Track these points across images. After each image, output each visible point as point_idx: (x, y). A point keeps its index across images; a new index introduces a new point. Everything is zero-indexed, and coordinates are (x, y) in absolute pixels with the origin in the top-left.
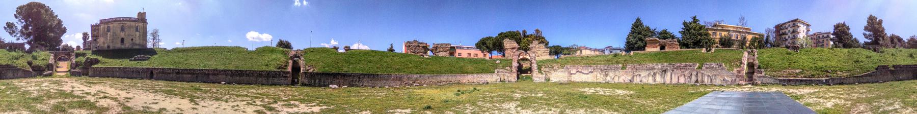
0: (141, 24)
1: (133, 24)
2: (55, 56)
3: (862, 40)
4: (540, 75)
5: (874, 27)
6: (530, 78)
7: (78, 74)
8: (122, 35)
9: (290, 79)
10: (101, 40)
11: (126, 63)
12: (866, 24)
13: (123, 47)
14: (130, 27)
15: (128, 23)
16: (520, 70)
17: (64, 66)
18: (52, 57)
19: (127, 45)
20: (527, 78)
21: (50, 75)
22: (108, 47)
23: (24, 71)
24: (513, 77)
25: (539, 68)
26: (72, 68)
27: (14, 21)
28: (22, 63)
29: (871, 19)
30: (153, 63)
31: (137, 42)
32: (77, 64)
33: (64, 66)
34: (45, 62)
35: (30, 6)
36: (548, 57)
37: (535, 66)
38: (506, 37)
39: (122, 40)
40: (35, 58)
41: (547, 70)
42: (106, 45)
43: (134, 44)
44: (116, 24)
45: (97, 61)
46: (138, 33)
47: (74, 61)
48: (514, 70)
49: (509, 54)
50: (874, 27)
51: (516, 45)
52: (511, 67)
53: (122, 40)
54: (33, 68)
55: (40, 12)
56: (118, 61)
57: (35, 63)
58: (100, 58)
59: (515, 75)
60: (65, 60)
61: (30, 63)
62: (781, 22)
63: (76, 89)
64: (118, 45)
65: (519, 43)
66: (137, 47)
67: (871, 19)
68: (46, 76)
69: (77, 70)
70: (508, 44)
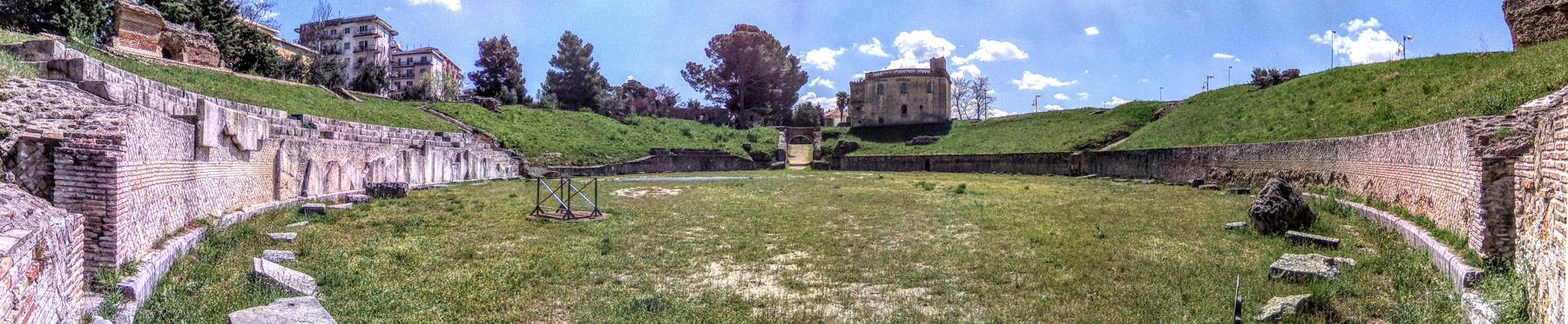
0: (935, 80)
1: (922, 80)
2: (787, 135)
3: (535, 100)
5: (573, 54)
7: (825, 167)
8: (904, 99)
9: (1505, 179)
10: (867, 109)
11: (901, 149)
12: (555, 51)
13: (905, 120)
14: (916, 85)
15: (914, 79)
17: (800, 155)
18: (782, 138)
19: (913, 116)
21: (782, 167)
22: (881, 120)
23: (742, 160)
26: (815, 157)
28: (733, 146)
29: (569, 41)
30: (941, 147)
31: (930, 111)
32: (824, 152)
33: (800, 155)
34: (770, 147)
35: (574, 37)
39: (904, 109)
40: (752, 139)
42: (876, 118)
43: (924, 115)
44: (891, 81)
45: (855, 147)
46: (930, 96)
47: (819, 147)
50: (573, 54)
53: (904, 109)
54: (752, 155)
55: (756, 53)
56: (888, 146)
57: (755, 147)
58: (858, 141)
60: (802, 141)
61: (747, 148)
64: (897, 118)
66: (931, 120)
67: (569, 41)
68: (775, 168)
69: (823, 161)
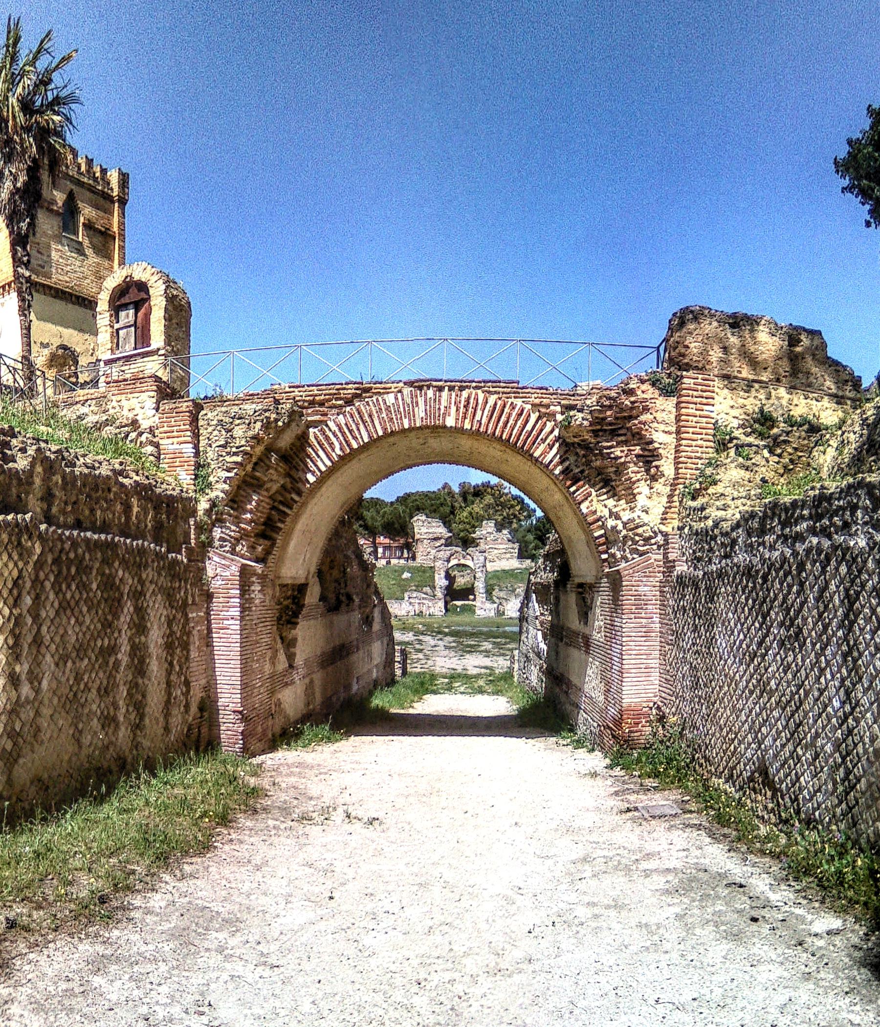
4: (488, 605)
6: (471, 610)
16: (453, 593)
20: (464, 608)
24: (437, 608)
25: (489, 592)
27: (868, 218)
36: (514, 564)
37: (480, 586)
38: (419, 509)
41: (502, 594)
48: (439, 594)
49: (425, 554)
51: (441, 530)
52: (433, 587)
59: (441, 604)
62: (823, 334)
63: (78, 263)
65: (447, 524)
70: (425, 528)
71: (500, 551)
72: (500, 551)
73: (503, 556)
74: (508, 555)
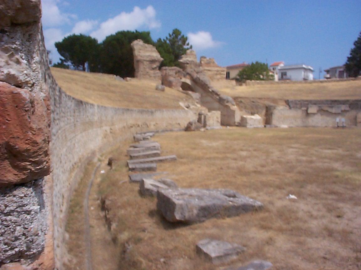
71: (212, 73)
72: (212, 73)
73: (215, 77)
74: (219, 76)
